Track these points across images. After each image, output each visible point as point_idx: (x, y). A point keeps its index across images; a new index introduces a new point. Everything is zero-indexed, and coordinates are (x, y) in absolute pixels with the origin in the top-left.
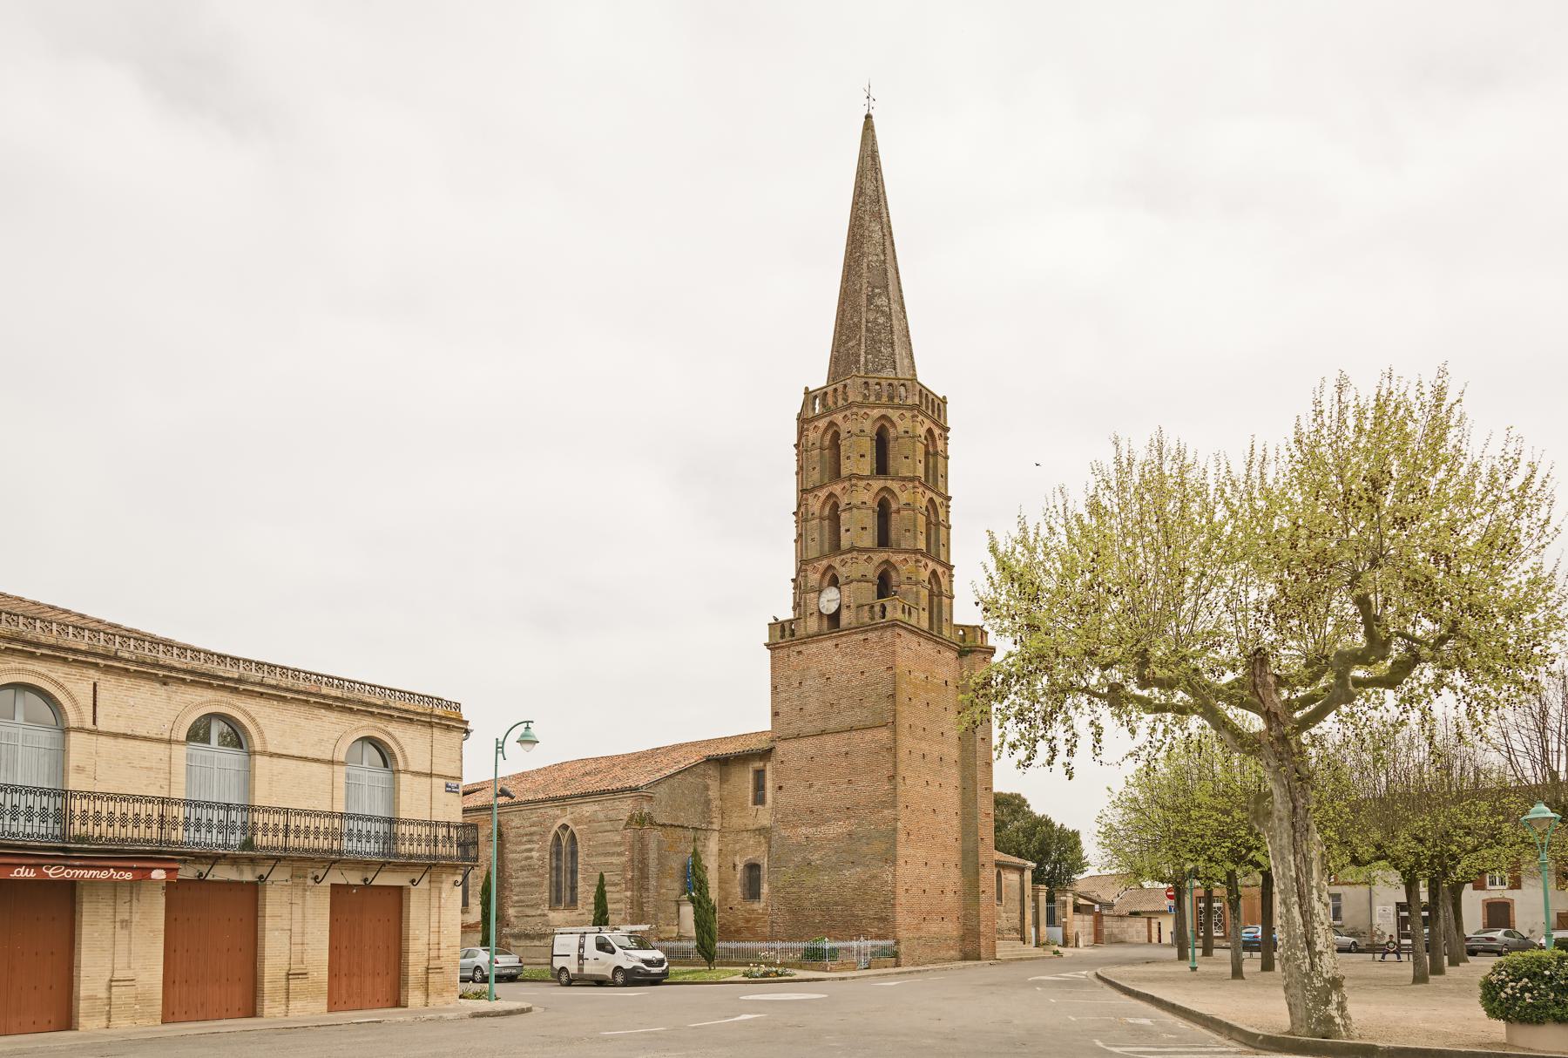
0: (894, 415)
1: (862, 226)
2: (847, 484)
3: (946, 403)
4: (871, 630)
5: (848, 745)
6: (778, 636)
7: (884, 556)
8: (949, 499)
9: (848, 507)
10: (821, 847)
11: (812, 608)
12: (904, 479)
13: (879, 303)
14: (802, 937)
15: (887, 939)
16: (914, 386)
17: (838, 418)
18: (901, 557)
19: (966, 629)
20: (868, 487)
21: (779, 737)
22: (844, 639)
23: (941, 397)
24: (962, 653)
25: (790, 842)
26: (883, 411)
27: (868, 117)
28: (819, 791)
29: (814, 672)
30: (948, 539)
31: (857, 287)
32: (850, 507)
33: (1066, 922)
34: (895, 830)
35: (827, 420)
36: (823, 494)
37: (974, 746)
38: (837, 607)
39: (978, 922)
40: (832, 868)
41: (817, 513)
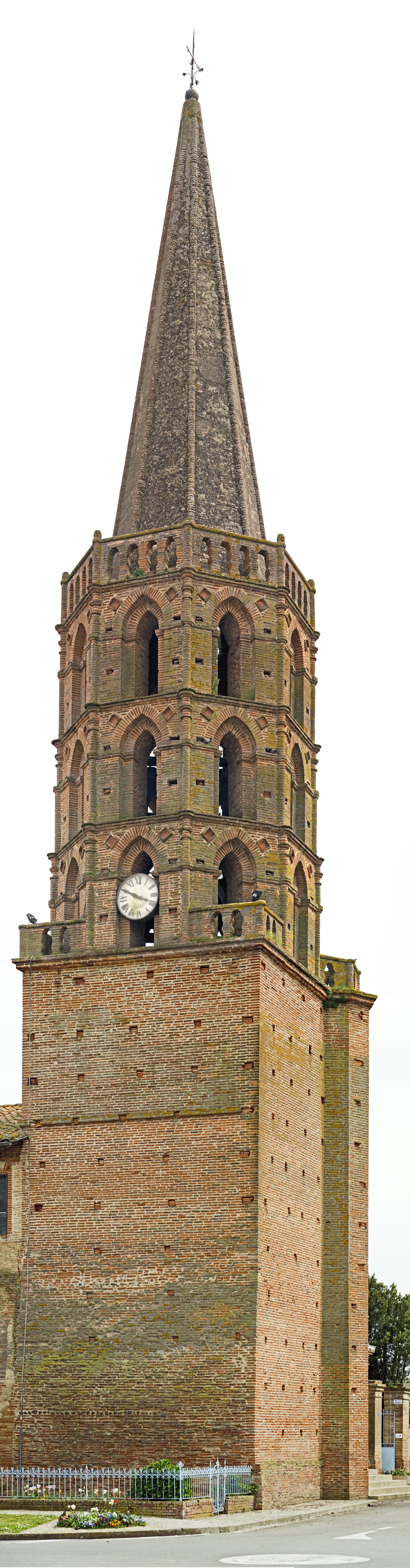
0: (250, 600)
1: (186, 276)
2: (172, 704)
3: (314, 592)
4: (216, 953)
5: (170, 1141)
6: (39, 950)
7: (232, 832)
8: (316, 749)
9: (174, 743)
10: (116, 1310)
11: (106, 906)
12: (263, 708)
13: (215, 410)
14: (80, 1460)
15: (237, 1464)
16: (280, 557)
17: (159, 592)
18: (259, 836)
19: (335, 965)
20: (207, 714)
21: (37, 1121)
22: (164, 964)
23: (307, 579)
24: (329, 1004)
25: (56, 1299)
26: (233, 592)
27: (191, 96)
28: (113, 1215)
29: (106, 1014)
30: (314, 815)
31: (179, 376)
32: (177, 743)
33: (401, 1440)
34: (254, 1285)
35: (139, 591)
36: (127, 716)
37: (346, 1154)
38: (151, 908)
39: (347, 1438)
40: (136, 1346)
41: (115, 747)
